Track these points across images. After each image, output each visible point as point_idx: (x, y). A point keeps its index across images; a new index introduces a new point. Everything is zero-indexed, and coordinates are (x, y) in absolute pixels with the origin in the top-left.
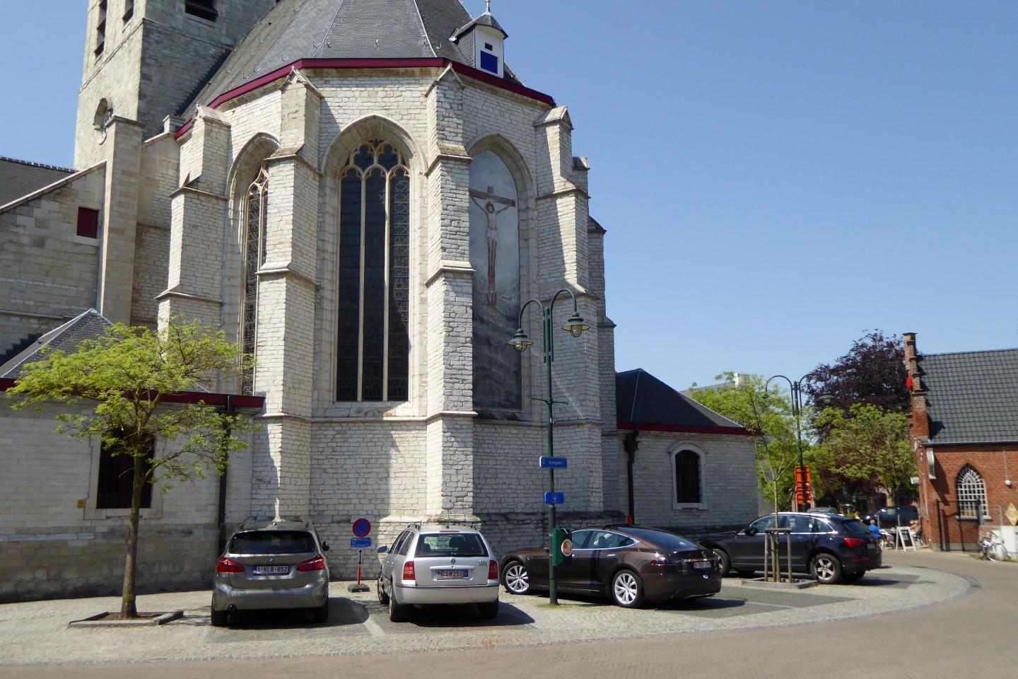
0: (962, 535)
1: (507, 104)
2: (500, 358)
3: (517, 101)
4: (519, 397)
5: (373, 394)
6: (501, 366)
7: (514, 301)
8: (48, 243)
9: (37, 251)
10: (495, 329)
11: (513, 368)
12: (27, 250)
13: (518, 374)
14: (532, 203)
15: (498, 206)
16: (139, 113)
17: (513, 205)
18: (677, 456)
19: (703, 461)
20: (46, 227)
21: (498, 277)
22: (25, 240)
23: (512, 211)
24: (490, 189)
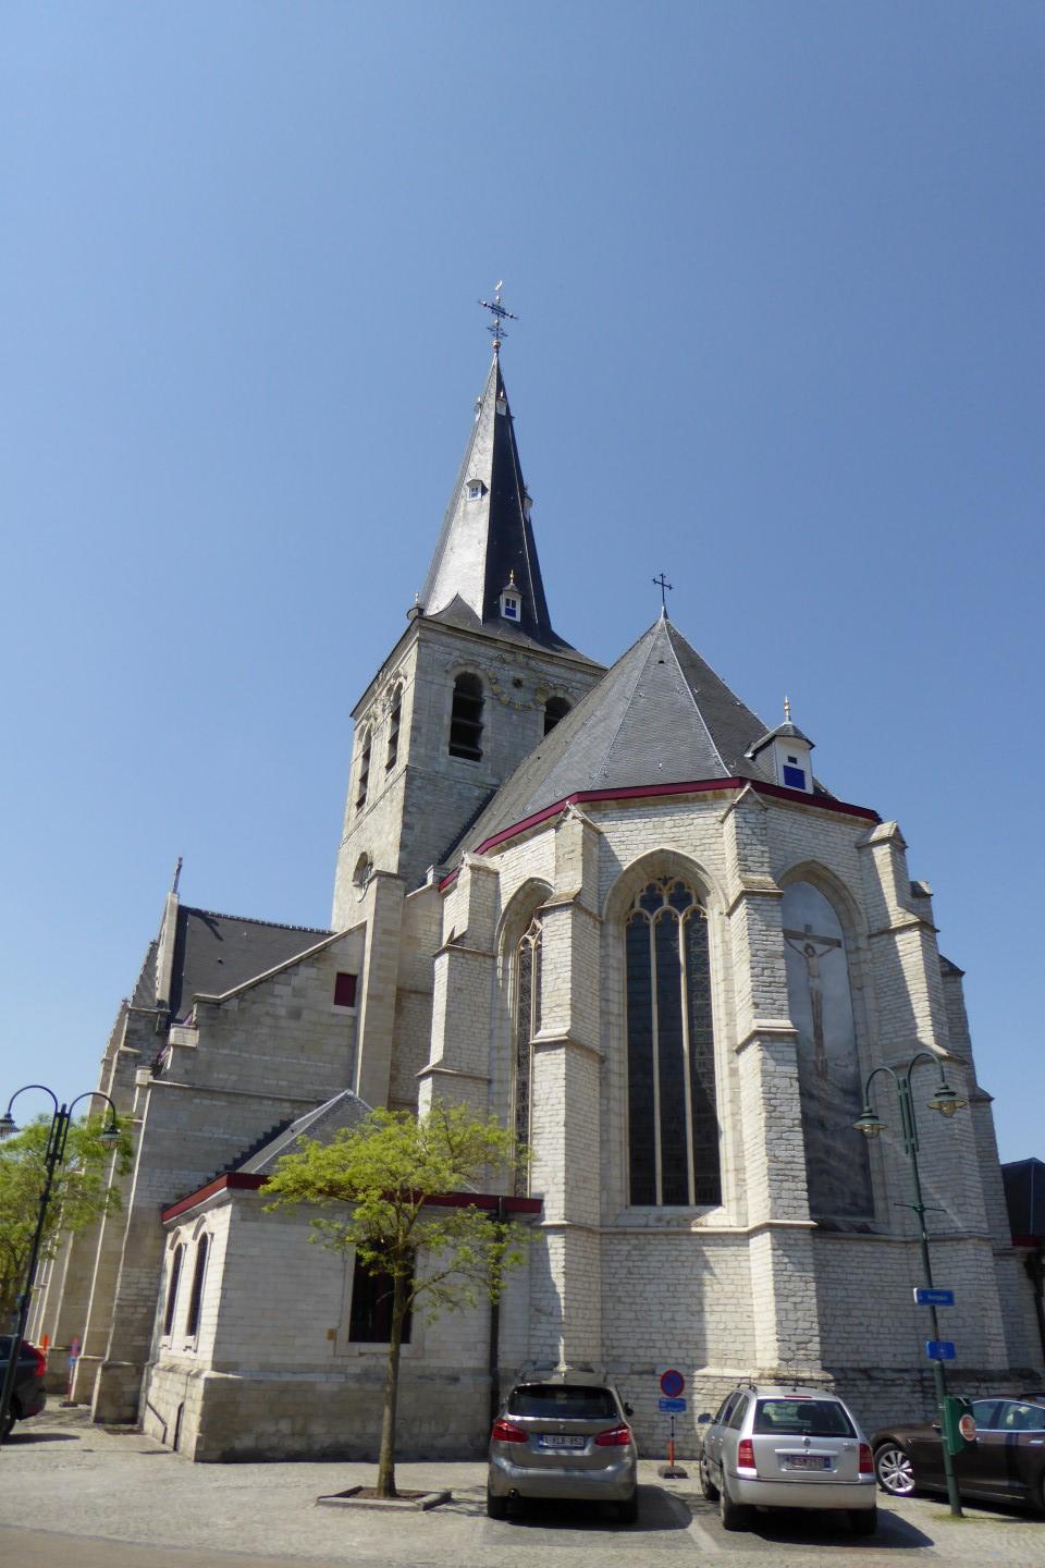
2: (840, 1146)
3: (831, 819)
4: (870, 1200)
7: (852, 1069)
8: (305, 1014)
14: (863, 943)
15: (820, 948)
17: (839, 944)
21: (828, 1037)
23: (839, 953)
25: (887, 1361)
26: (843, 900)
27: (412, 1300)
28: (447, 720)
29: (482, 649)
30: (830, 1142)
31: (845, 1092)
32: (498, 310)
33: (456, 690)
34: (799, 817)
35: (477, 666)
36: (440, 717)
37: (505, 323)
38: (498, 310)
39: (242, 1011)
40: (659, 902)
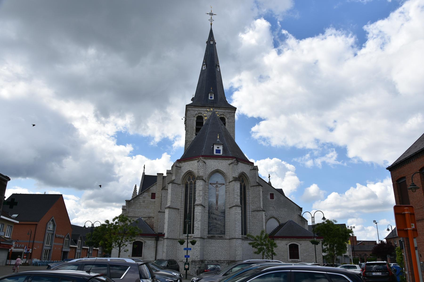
0: (34, 238)
1: (221, 161)
2: (219, 222)
3: (223, 159)
4: (225, 232)
5: (189, 233)
6: (219, 224)
7: (224, 208)
8: (146, 202)
9: (143, 203)
10: (218, 215)
11: (223, 225)
12: (142, 203)
13: (224, 226)
14: (228, 184)
15: (219, 186)
16: (97, 227)
17: (224, 184)
18: (289, 245)
19: (299, 247)
20: (381, 38)
21: (219, 203)
22: (141, 201)
23: (224, 186)
24: (217, 182)
25: (222, 259)
26: (225, 176)
27: (17, 188)
28: (195, 128)
29: (203, 109)
30: (217, 222)
31: (222, 212)
32: (211, 14)
33: (196, 120)
34: (215, 160)
35: (201, 113)
36: (193, 127)
37: (213, 17)
38: (211, 14)
39: (134, 202)
40: (190, 180)
